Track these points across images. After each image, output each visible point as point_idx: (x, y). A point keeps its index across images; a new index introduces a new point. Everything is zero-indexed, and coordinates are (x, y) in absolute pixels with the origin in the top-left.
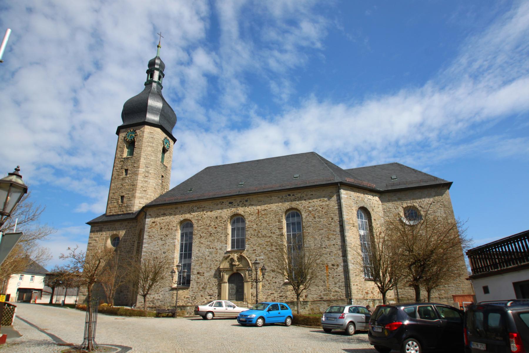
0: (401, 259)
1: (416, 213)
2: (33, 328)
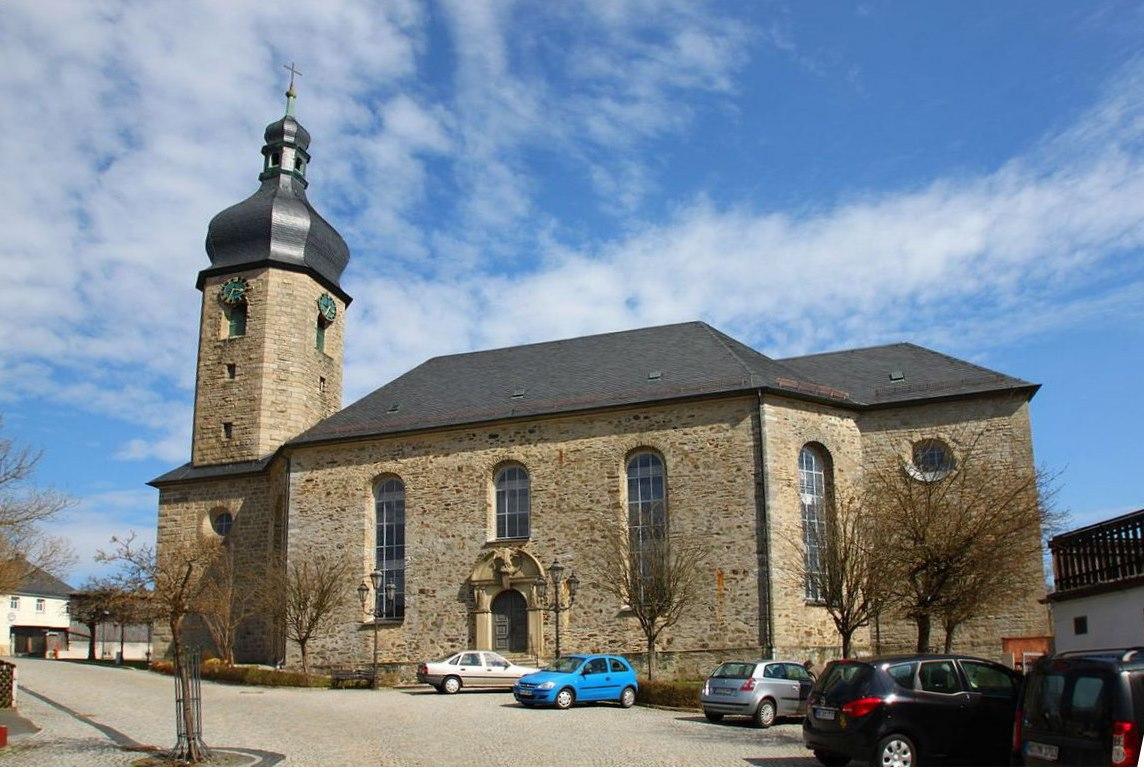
0: (894, 557)
1: (942, 454)
2: (61, 712)
